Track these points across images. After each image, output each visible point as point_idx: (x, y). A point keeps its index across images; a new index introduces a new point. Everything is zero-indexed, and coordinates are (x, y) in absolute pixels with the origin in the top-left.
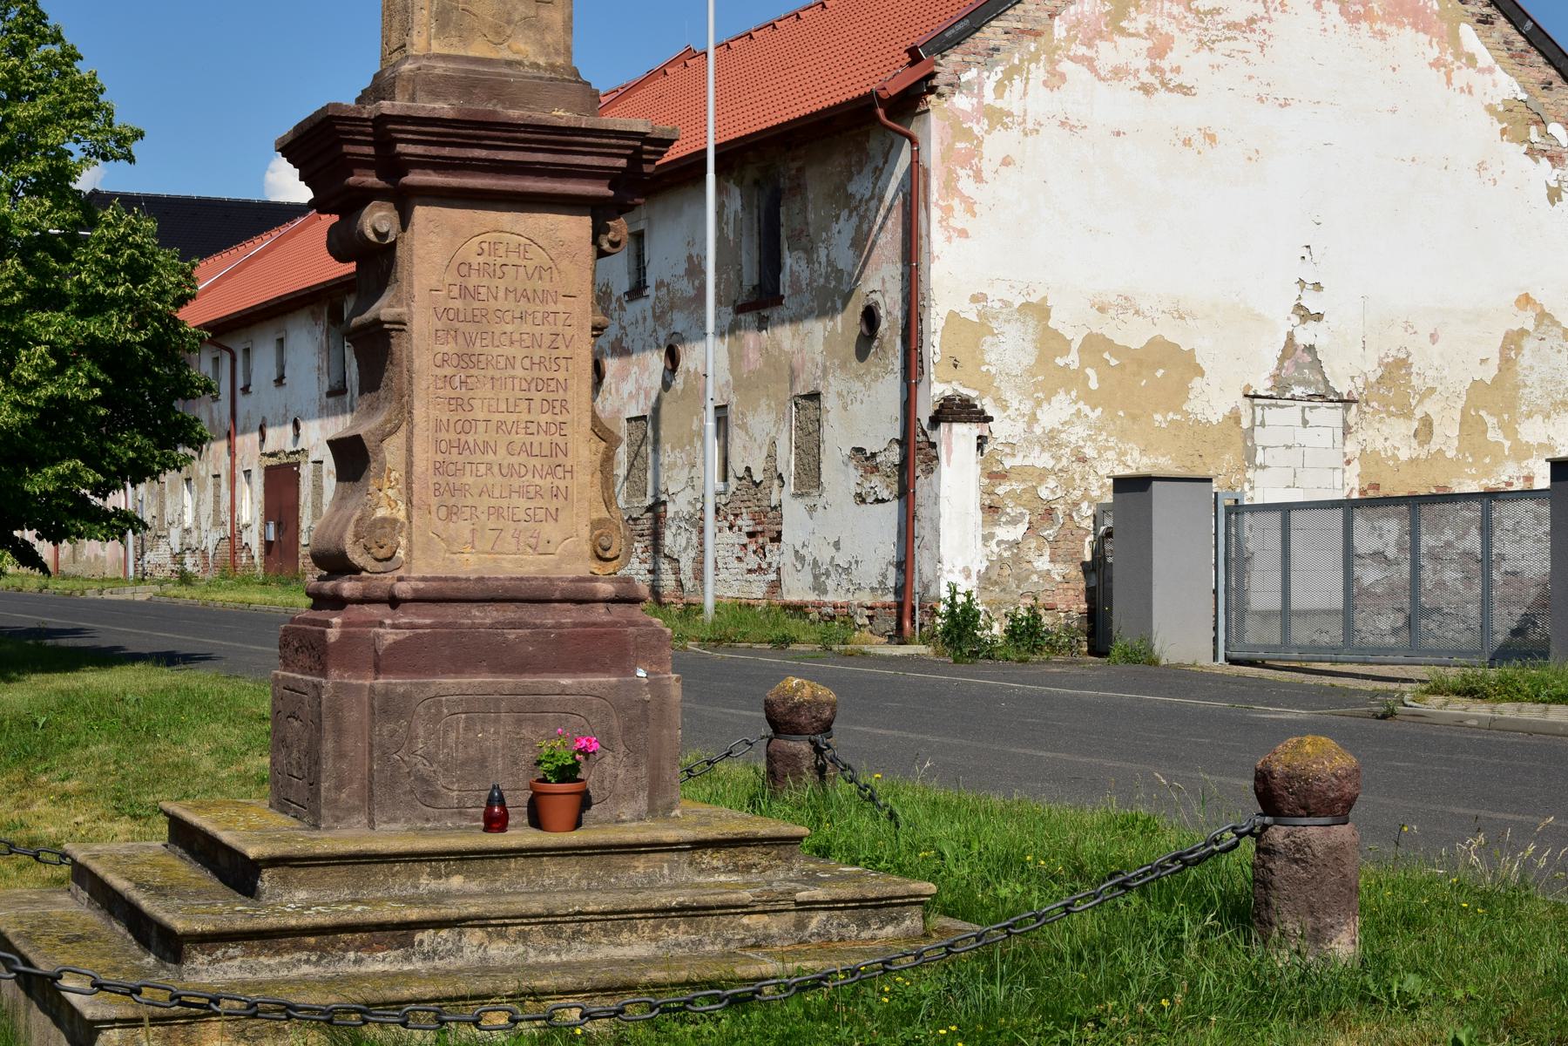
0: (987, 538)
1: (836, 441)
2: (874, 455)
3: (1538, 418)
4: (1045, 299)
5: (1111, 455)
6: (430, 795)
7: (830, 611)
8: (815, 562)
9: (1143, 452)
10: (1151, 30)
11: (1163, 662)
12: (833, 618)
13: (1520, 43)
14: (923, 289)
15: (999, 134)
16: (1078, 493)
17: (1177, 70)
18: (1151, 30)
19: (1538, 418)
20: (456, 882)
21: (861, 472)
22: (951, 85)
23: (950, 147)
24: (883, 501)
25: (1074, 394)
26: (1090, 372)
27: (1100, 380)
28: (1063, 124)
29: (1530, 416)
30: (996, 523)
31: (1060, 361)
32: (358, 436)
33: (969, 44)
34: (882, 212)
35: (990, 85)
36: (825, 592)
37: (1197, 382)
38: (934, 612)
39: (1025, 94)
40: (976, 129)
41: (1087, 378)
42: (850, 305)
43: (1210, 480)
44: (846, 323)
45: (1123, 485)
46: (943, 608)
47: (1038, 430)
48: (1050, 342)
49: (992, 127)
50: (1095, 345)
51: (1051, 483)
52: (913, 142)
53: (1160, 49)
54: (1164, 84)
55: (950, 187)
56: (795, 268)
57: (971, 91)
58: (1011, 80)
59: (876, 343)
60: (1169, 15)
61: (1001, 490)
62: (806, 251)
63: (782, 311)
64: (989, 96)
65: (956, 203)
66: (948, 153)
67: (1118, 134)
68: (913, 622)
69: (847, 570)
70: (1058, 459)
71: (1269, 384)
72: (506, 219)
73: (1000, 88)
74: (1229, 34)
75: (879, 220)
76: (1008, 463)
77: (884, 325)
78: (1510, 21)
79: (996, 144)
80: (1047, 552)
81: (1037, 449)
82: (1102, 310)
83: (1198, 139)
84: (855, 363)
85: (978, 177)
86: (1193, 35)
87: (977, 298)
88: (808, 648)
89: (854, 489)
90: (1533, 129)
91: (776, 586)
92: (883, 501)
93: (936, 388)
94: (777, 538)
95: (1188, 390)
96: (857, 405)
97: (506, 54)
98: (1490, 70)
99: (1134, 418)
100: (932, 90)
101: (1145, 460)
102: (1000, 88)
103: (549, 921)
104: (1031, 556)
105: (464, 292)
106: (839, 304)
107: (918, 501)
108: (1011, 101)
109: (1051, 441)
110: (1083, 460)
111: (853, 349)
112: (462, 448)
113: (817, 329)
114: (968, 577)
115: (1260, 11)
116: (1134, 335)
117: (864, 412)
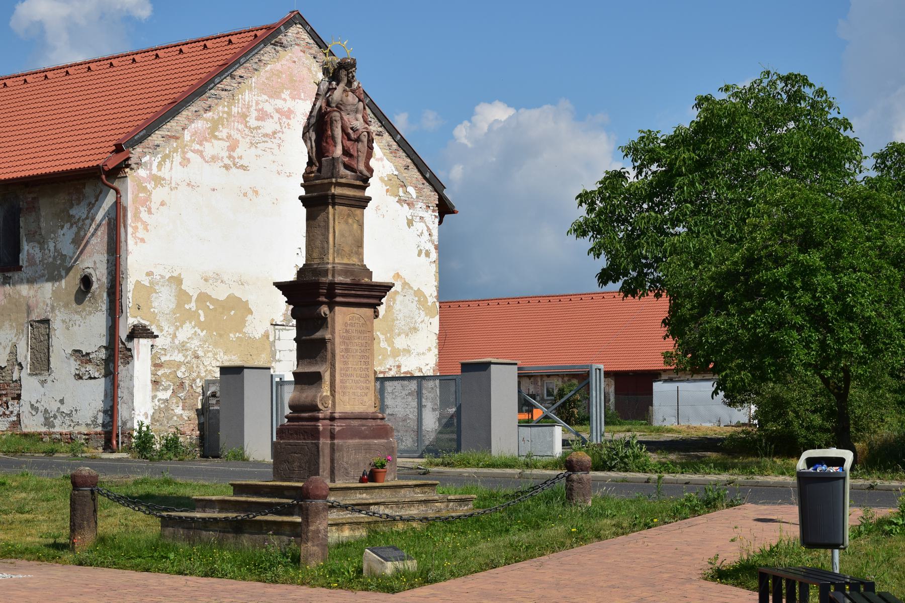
0: (154, 397)
1: (61, 344)
2: (88, 354)
3: (403, 336)
4: (180, 274)
5: (210, 355)
6: (347, 474)
7: (58, 436)
8: (46, 411)
9: (225, 353)
10: (229, 137)
11: (251, 459)
12: (60, 440)
13: (395, 146)
14: (122, 268)
15: (159, 189)
16: (195, 374)
17: (240, 158)
18: (229, 137)
19: (403, 336)
20: (364, 495)
21: (79, 362)
22: (137, 164)
23: (137, 196)
24: (95, 378)
25: (193, 323)
26: (200, 312)
27: (205, 316)
28: (188, 184)
29: (399, 335)
30: (157, 390)
31: (187, 307)
32: (319, 373)
33: (145, 143)
34: (94, 226)
35: (155, 164)
36: (54, 426)
37: (249, 318)
38: (131, 436)
39: (171, 169)
40: (149, 187)
41: (199, 315)
42: (71, 274)
43: (269, 368)
44: (70, 284)
45: (224, 370)
46: (135, 434)
47: (177, 342)
48: (182, 297)
49: (156, 186)
50: (203, 298)
51: (183, 369)
52: (117, 192)
53: (232, 148)
54: (235, 165)
55: (137, 217)
56: (31, 251)
57: (146, 167)
58: (165, 161)
59: (90, 295)
60: (238, 129)
61: (159, 373)
62: (39, 243)
63: (22, 275)
64: (155, 170)
65: (139, 224)
66: (136, 198)
67: (214, 190)
68: (118, 442)
69: (70, 415)
70: (186, 357)
71: (282, 318)
72: (355, 310)
73: (160, 165)
74: (264, 139)
75: (92, 230)
76: (163, 359)
77: (95, 286)
78: (391, 135)
79: (159, 194)
80: (181, 404)
81: (177, 351)
82: (206, 280)
83: (250, 193)
84: (74, 305)
85: (150, 211)
86: (248, 140)
87: (149, 274)
88: (65, 455)
89: (73, 372)
90: (401, 189)
91: (18, 422)
92: (95, 378)
93: (130, 320)
94: (18, 397)
95: (245, 321)
96: (76, 328)
97: (351, 262)
98: (382, 160)
99: (221, 336)
100: (128, 166)
101: (226, 357)
102: (160, 165)
103: (397, 503)
104: (174, 407)
105: (347, 331)
106: (63, 273)
107: (120, 378)
108: (165, 173)
109: (183, 348)
110: (197, 357)
111: (73, 298)
112: (346, 375)
113: (48, 288)
114: (147, 418)
115: (279, 128)
116: (220, 293)
117: (86, 330)
